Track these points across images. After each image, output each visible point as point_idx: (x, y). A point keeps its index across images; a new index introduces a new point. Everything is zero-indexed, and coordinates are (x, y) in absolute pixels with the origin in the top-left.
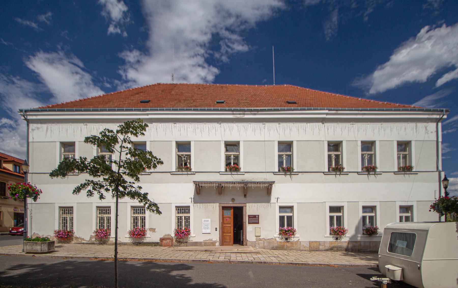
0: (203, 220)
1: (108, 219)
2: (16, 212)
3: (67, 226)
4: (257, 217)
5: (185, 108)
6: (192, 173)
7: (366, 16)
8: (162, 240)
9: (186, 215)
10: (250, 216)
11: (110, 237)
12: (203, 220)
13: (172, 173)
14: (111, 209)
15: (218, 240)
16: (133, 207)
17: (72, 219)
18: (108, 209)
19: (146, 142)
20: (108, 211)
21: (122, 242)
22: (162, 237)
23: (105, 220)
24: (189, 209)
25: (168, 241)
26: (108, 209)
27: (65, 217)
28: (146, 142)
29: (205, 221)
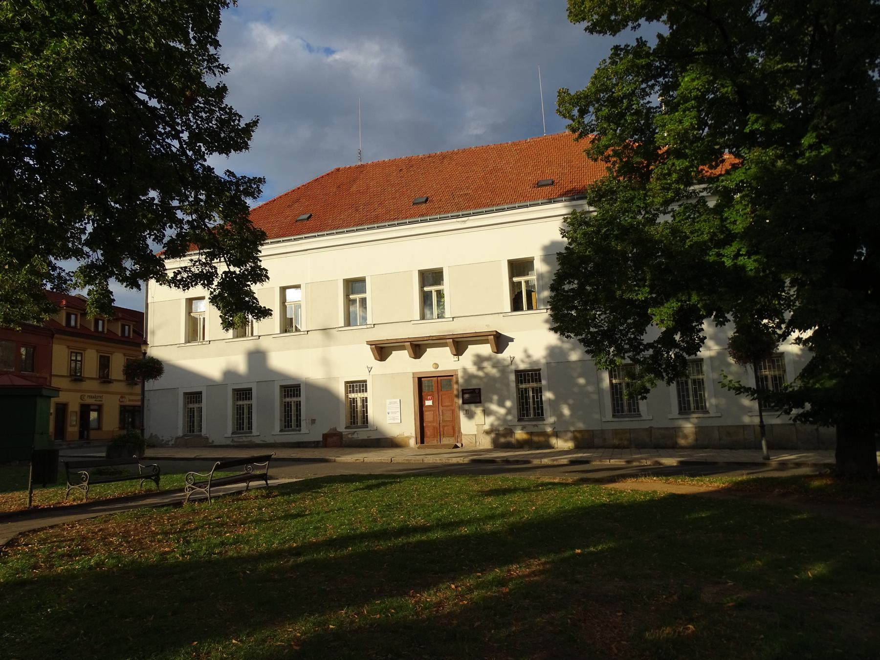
0: (388, 401)
1: (249, 407)
2: (122, 404)
3: (193, 421)
4: (477, 391)
5: (540, 202)
6: (368, 326)
7: (759, 10)
8: (325, 436)
9: (295, 399)
10: (465, 391)
11: (545, 422)
12: (388, 401)
13: (179, 345)
14: (368, 383)
15: (414, 434)
16: (285, 388)
17: (200, 410)
18: (363, 385)
19: (442, 269)
20: (363, 387)
21: (268, 442)
22: (326, 431)
23: (195, 411)
24: (366, 385)
25: (335, 438)
26: (363, 385)
27: (191, 409)
28: (442, 269)
29: (390, 403)
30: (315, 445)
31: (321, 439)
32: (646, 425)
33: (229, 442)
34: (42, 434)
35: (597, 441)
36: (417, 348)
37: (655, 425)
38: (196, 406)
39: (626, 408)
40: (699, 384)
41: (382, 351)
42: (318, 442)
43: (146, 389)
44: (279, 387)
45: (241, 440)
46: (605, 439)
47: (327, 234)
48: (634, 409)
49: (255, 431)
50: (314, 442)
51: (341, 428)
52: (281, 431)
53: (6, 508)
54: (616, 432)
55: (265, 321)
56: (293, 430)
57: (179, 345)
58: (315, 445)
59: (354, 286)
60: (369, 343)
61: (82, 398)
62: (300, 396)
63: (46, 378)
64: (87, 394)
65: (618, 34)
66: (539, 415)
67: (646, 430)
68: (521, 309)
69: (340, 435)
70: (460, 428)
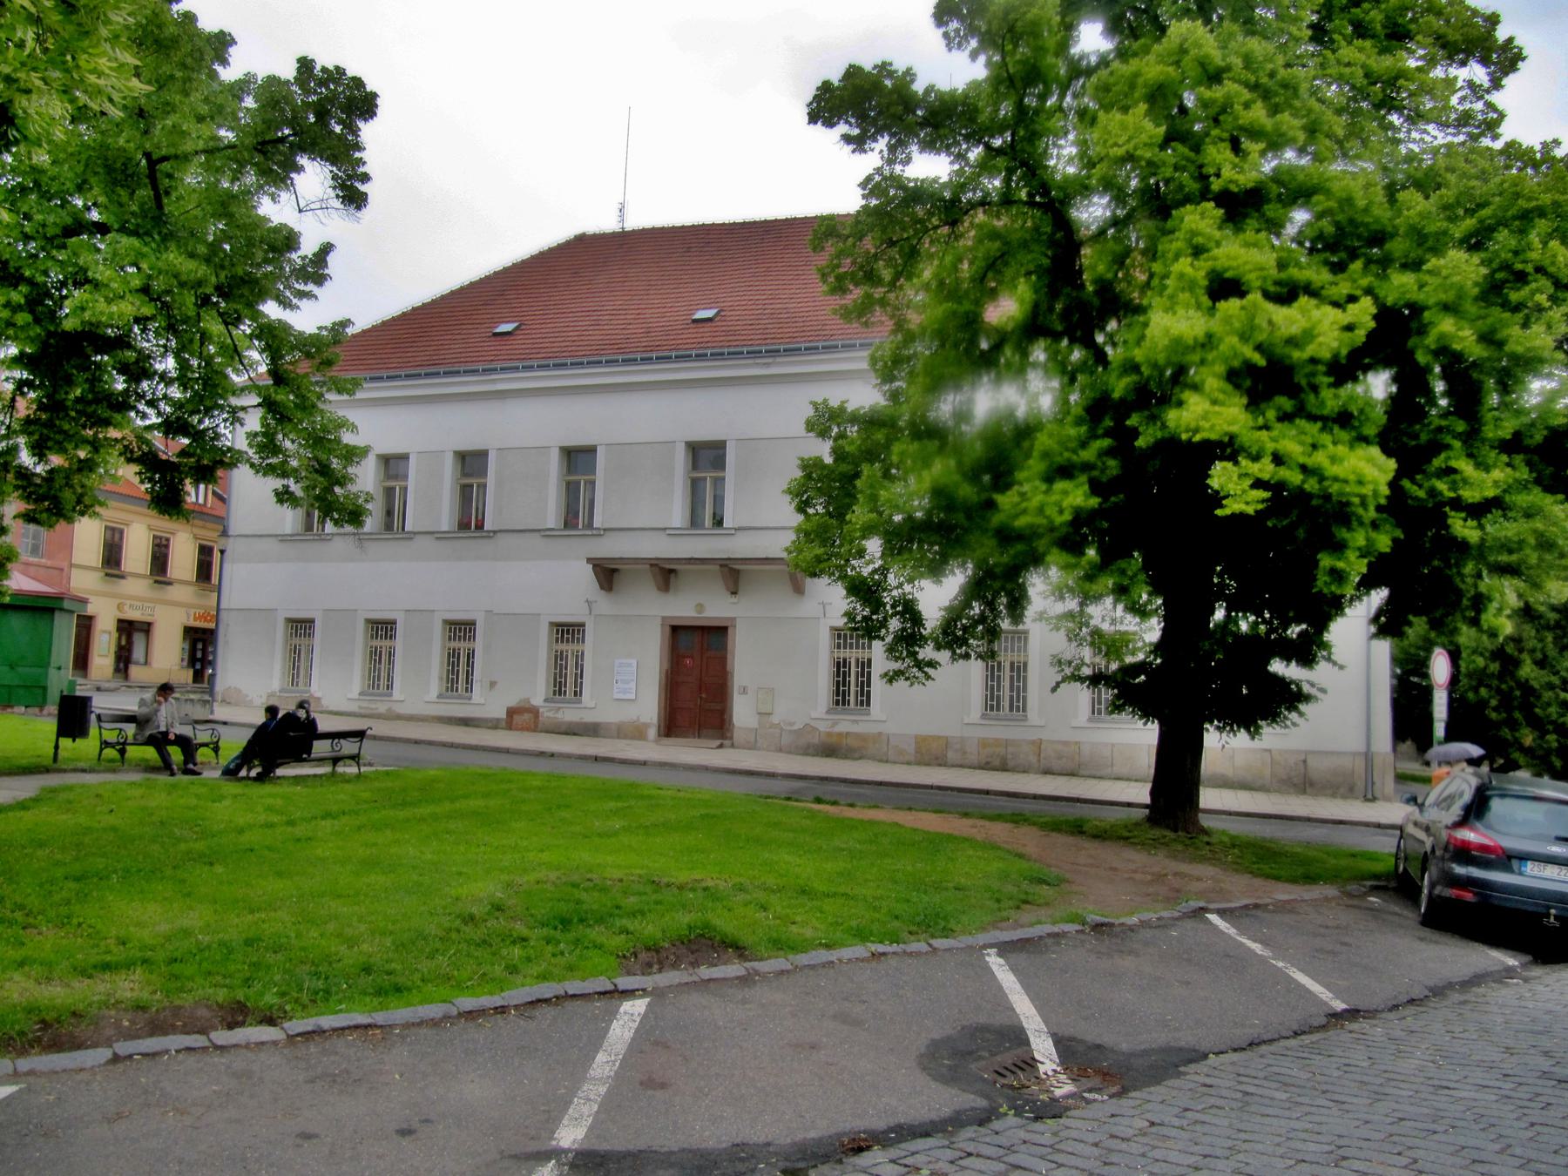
0: (617, 662)
8: (511, 712)
13: (546, 533)
15: (655, 720)
18: (568, 631)
25: (526, 716)
30: (494, 725)
31: (504, 716)
32: (1033, 735)
33: (353, 707)
34: (59, 668)
35: (951, 756)
36: (666, 574)
37: (1045, 735)
38: (386, 643)
39: (1007, 704)
40: (1020, 670)
41: (608, 574)
42: (498, 720)
43: (223, 606)
44: (440, 622)
45: (373, 706)
46: (965, 753)
47: (427, 375)
48: (1018, 707)
49: (397, 693)
50: (491, 720)
51: (538, 700)
52: (440, 696)
53: (1564, 870)
54: (984, 743)
55: (14, 513)
56: (460, 697)
57: (546, 533)
58: (494, 725)
59: (578, 458)
60: (589, 560)
61: (120, 607)
62: (583, 642)
63: (62, 570)
64: (128, 602)
65: (819, 128)
66: (992, 709)
67: (1033, 742)
68: (575, 527)
69: (535, 712)
70: (731, 716)
